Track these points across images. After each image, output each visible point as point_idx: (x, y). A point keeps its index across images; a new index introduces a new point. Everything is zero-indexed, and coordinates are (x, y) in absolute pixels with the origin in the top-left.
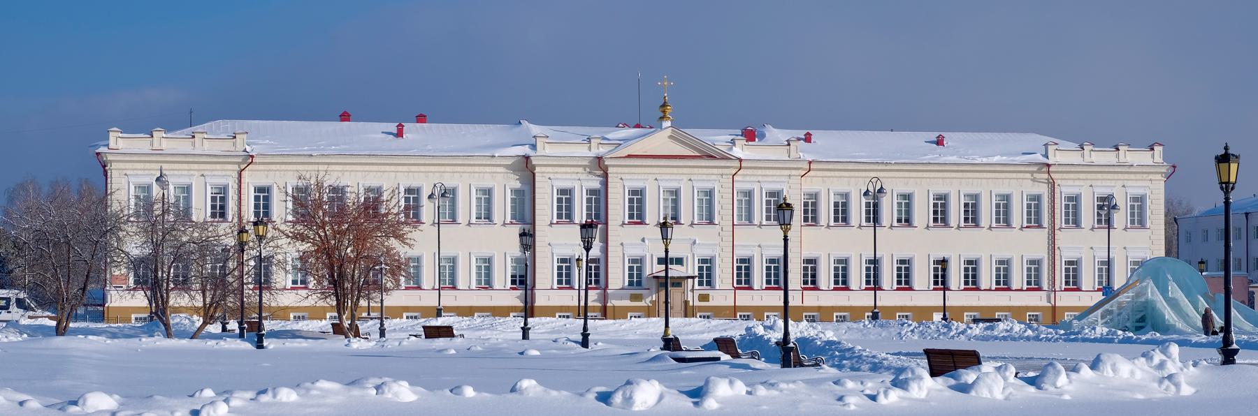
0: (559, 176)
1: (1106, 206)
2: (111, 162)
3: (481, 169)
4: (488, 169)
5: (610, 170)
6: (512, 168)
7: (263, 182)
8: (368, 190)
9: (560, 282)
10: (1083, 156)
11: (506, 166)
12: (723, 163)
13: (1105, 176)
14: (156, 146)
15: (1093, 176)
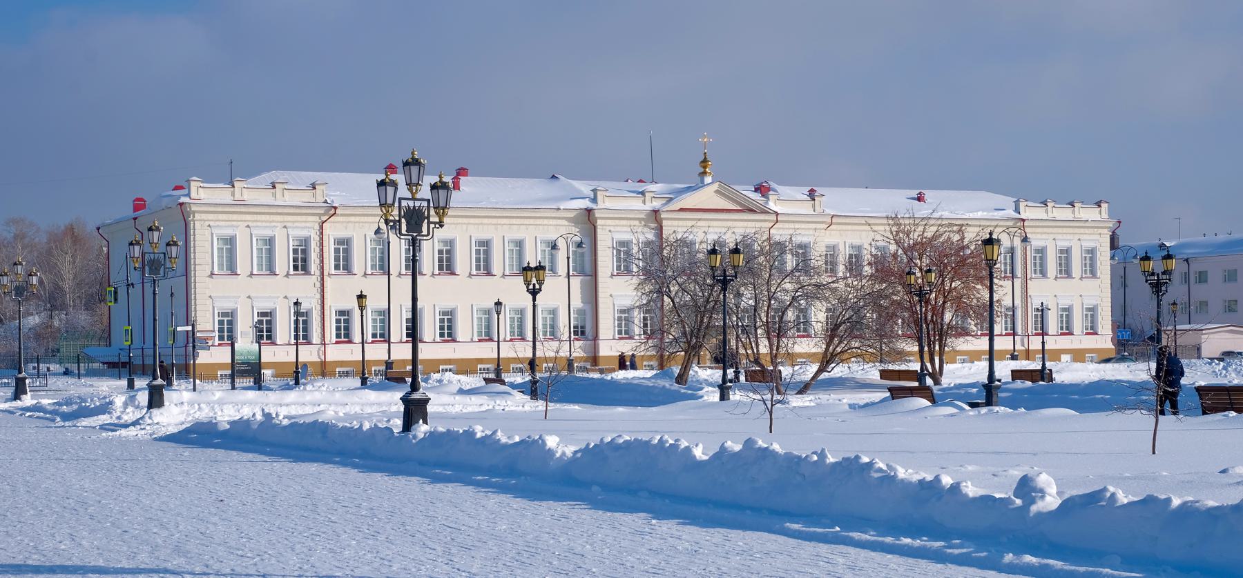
0: (619, 229)
1: (1065, 257)
2: (194, 212)
3: (546, 222)
4: (551, 222)
5: (665, 223)
6: (574, 221)
7: (343, 234)
8: (852, 247)
9: (442, 335)
10: (274, 195)
11: (640, 220)
12: (762, 217)
13: (1065, 230)
14: (238, 196)
15: (1056, 230)
